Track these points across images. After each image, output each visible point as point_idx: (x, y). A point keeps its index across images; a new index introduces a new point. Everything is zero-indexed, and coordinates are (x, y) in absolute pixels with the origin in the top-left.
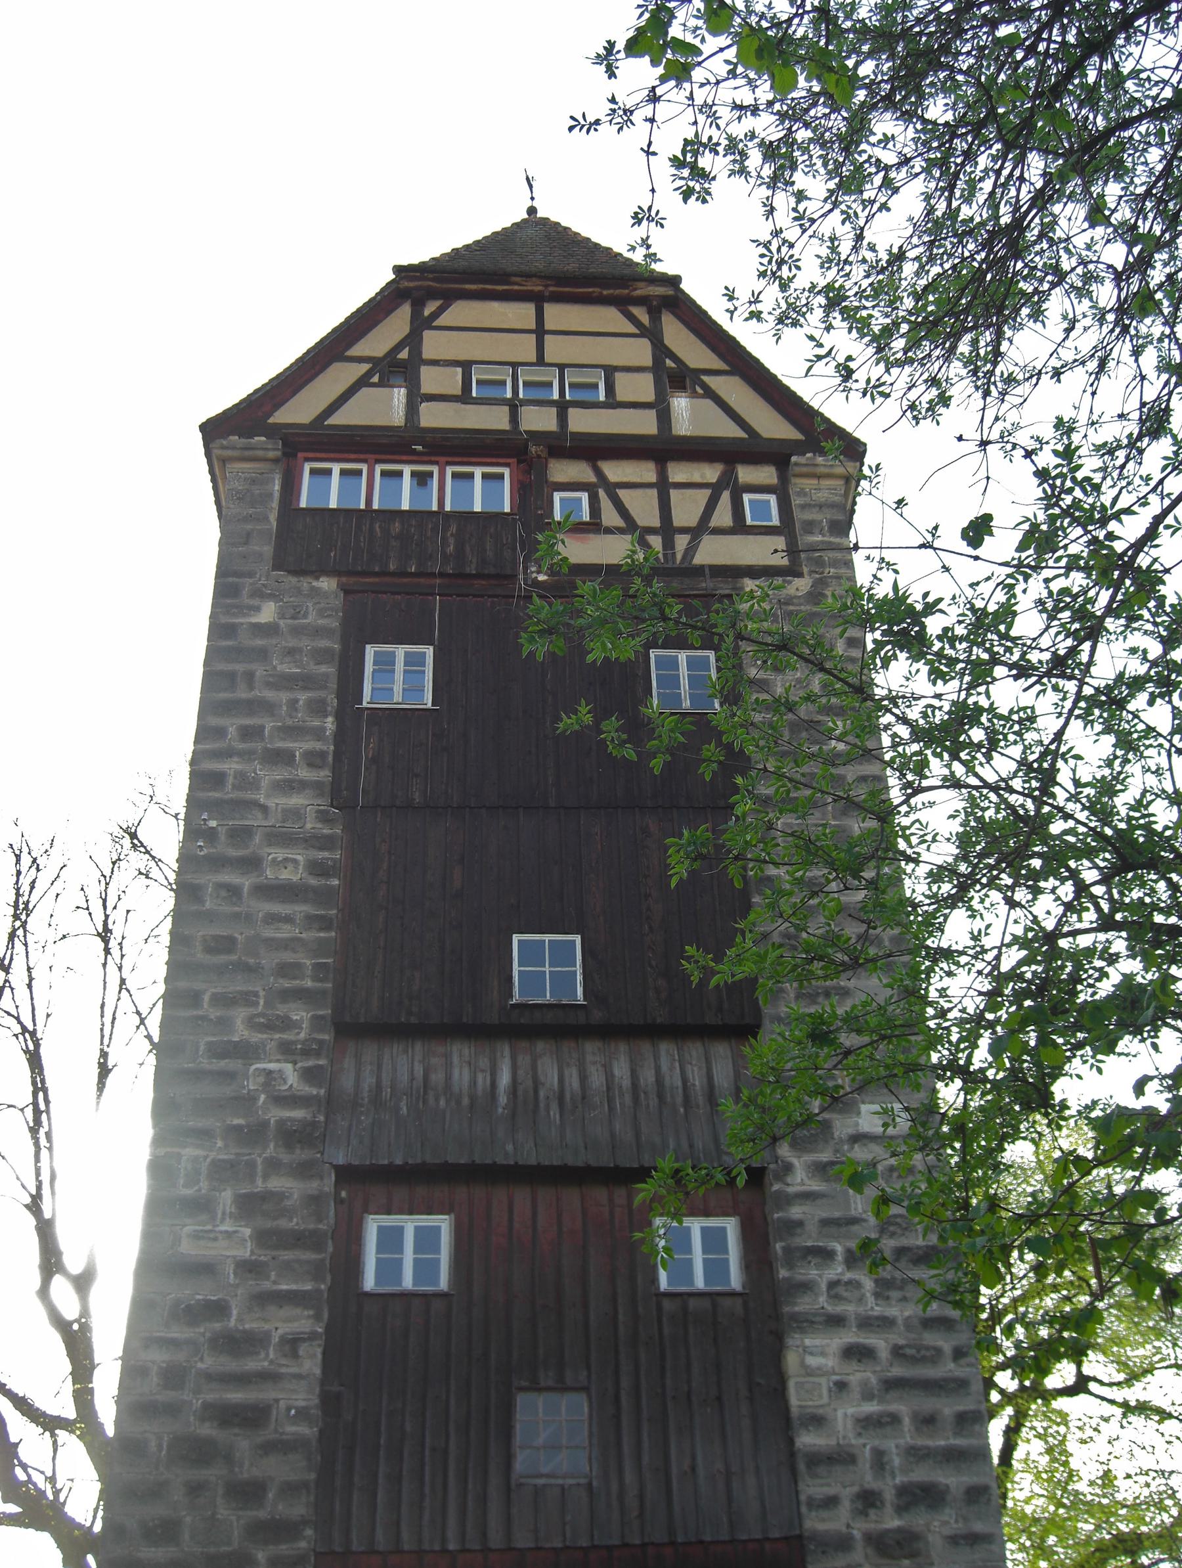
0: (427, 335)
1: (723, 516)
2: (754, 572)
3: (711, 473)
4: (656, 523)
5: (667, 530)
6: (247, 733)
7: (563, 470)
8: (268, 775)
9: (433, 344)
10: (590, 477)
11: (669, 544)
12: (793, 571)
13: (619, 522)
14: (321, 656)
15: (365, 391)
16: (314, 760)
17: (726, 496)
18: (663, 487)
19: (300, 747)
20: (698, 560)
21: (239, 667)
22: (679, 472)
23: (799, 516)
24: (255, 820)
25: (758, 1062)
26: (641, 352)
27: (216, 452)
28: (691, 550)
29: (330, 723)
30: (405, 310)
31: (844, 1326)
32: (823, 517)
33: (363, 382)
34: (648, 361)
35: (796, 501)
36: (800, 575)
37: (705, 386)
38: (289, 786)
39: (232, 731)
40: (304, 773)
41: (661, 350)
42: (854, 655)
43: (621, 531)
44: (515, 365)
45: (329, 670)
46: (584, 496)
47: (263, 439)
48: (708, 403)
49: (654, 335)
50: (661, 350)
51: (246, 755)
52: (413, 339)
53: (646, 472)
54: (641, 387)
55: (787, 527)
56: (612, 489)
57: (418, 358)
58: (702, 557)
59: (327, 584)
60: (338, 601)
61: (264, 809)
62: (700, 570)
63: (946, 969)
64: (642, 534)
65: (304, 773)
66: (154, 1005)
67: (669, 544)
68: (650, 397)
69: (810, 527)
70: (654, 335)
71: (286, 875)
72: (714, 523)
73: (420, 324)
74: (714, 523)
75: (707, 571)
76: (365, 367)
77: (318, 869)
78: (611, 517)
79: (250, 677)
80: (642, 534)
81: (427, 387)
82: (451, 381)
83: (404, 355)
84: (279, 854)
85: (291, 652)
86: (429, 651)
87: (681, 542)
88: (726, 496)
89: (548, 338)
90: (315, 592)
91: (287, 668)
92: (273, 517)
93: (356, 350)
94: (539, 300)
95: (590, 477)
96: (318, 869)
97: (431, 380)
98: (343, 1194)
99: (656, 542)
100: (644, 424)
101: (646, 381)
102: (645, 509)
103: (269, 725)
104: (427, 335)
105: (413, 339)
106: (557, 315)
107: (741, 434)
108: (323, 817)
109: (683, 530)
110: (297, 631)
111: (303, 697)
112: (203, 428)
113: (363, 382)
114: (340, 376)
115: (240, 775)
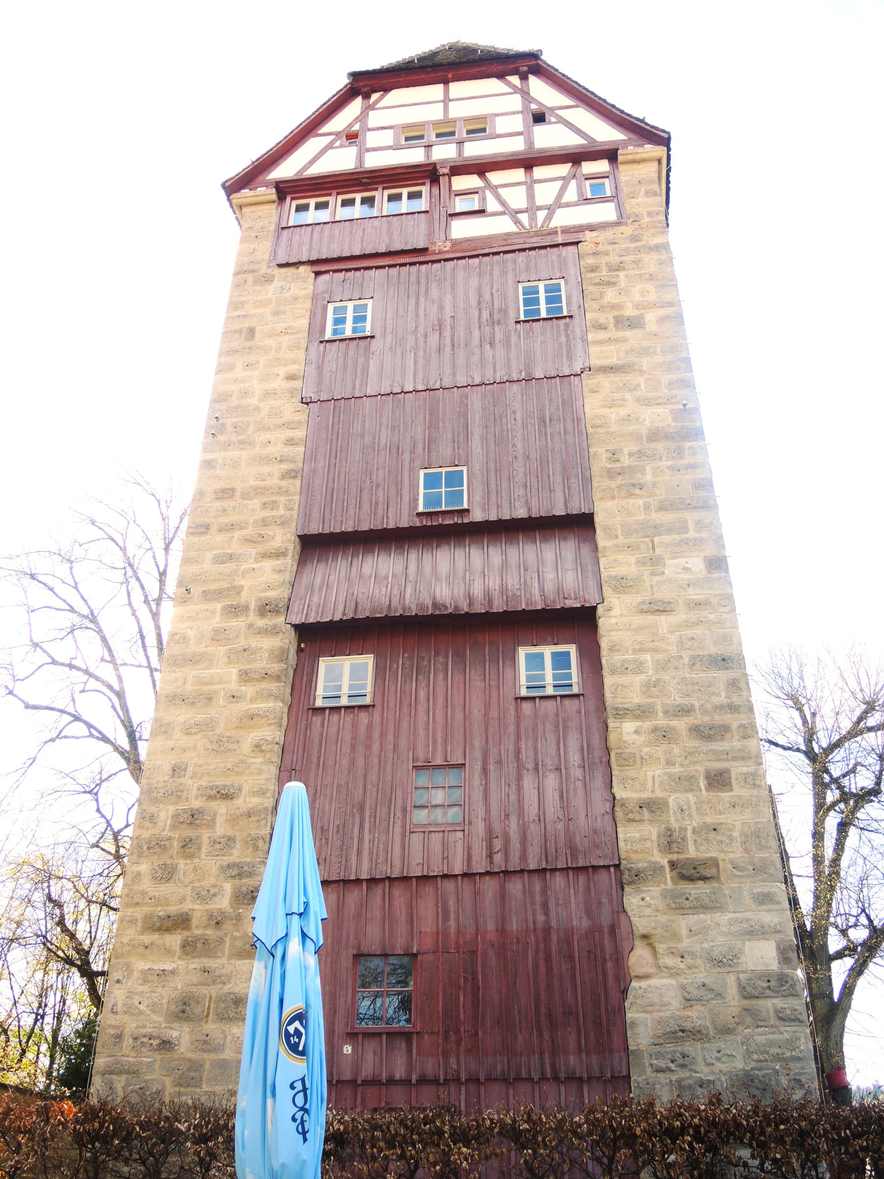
1: (571, 194)
2: (592, 228)
5: (532, 209)
13: (500, 209)
20: (552, 225)
22: (539, 172)
26: (515, 102)
27: (234, 201)
28: (549, 217)
30: (358, 101)
31: (637, 1025)
33: (330, 146)
37: (557, 116)
42: (593, 314)
47: (264, 188)
48: (560, 126)
52: (362, 117)
53: (518, 174)
54: (517, 123)
62: (554, 232)
63: (780, 684)
64: (514, 214)
66: (65, 601)
67: (533, 219)
68: (520, 128)
71: (270, 450)
72: (565, 200)
74: (565, 200)
75: (559, 230)
76: (332, 137)
80: (514, 214)
82: (387, 138)
88: (573, 182)
89: (442, 98)
96: (290, 442)
97: (372, 139)
98: (303, 645)
100: (516, 145)
104: (372, 113)
106: (458, 88)
107: (582, 141)
112: (223, 186)
113: (330, 146)
114: (312, 145)
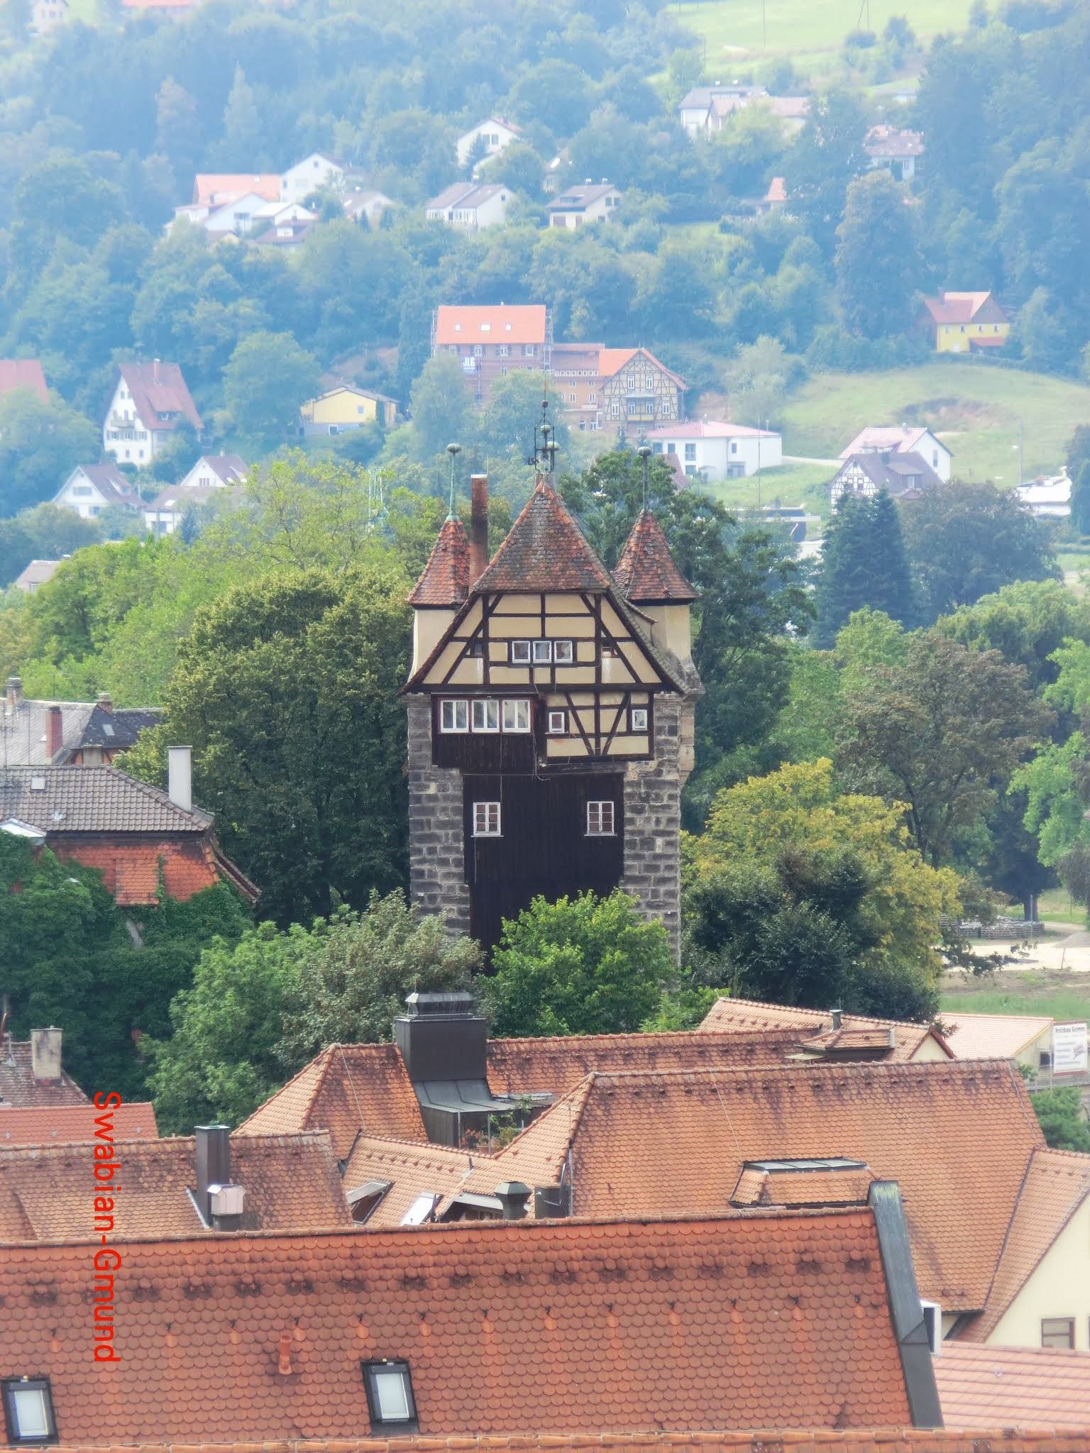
0: (492, 620)
1: (622, 727)
3: (618, 699)
4: (593, 731)
6: (432, 851)
7: (556, 701)
8: (440, 871)
9: (497, 627)
10: (564, 703)
11: (598, 744)
12: (648, 757)
14: (456, 810)
15: (465, 661)
16: (457, 863)
17: (625, 712)
18: (597, 708)
19: (451, 857)
20: (610, 752)
21: (424, 818)
23: (656, 723)
24: (437, 891)
25: (140, 786)
29: (462, 845)
32: (666, 724)
33: (462, 655)
34: (592, 634)
35: (656, 714)
36: (652, 759)
38: (448, 876)
39: (425, 850)
40: (454, 870)
41: (600, 626)
43: (577, 736)
44: (531, 640)
45: (459, 818)
46: (563, 714)
49: (595, 613)
50: (600, 626)
51: (431, 862)
52: (484, 625)
53: (589, 700)
55: (650, 732)
56: (575, 709)
57: (487, 639)
58: (612, 751)
59: (455, 772)
60: (460, 782)
61: (440, 886)
65: (454, 870)
69: (660, 730)
70: (595, 613)
73: (488, 612)
77: (461, 912)
78: (574, 729)
79: (429, 822)
81: (492, 658)
83: (480, 635)
84: (448, 906)
85: (444, 809)
86: (498, 805)
87: (603, 740)
88: (625, 712)
90: (451, 776)
91: (443, 818)
92: (430, 734)
93: (460, 633)
94: (543, 594)
95: (564, 703)
97: (497, 652)
99: (592, 741)
101: (591, 646)
102: (587, 718)
103: (439, 846)
105: (484, 625)
108: (462, 889)
109: (605, 735)
110: (446, 798)
111: (450, 832)
115: (430, 871)
